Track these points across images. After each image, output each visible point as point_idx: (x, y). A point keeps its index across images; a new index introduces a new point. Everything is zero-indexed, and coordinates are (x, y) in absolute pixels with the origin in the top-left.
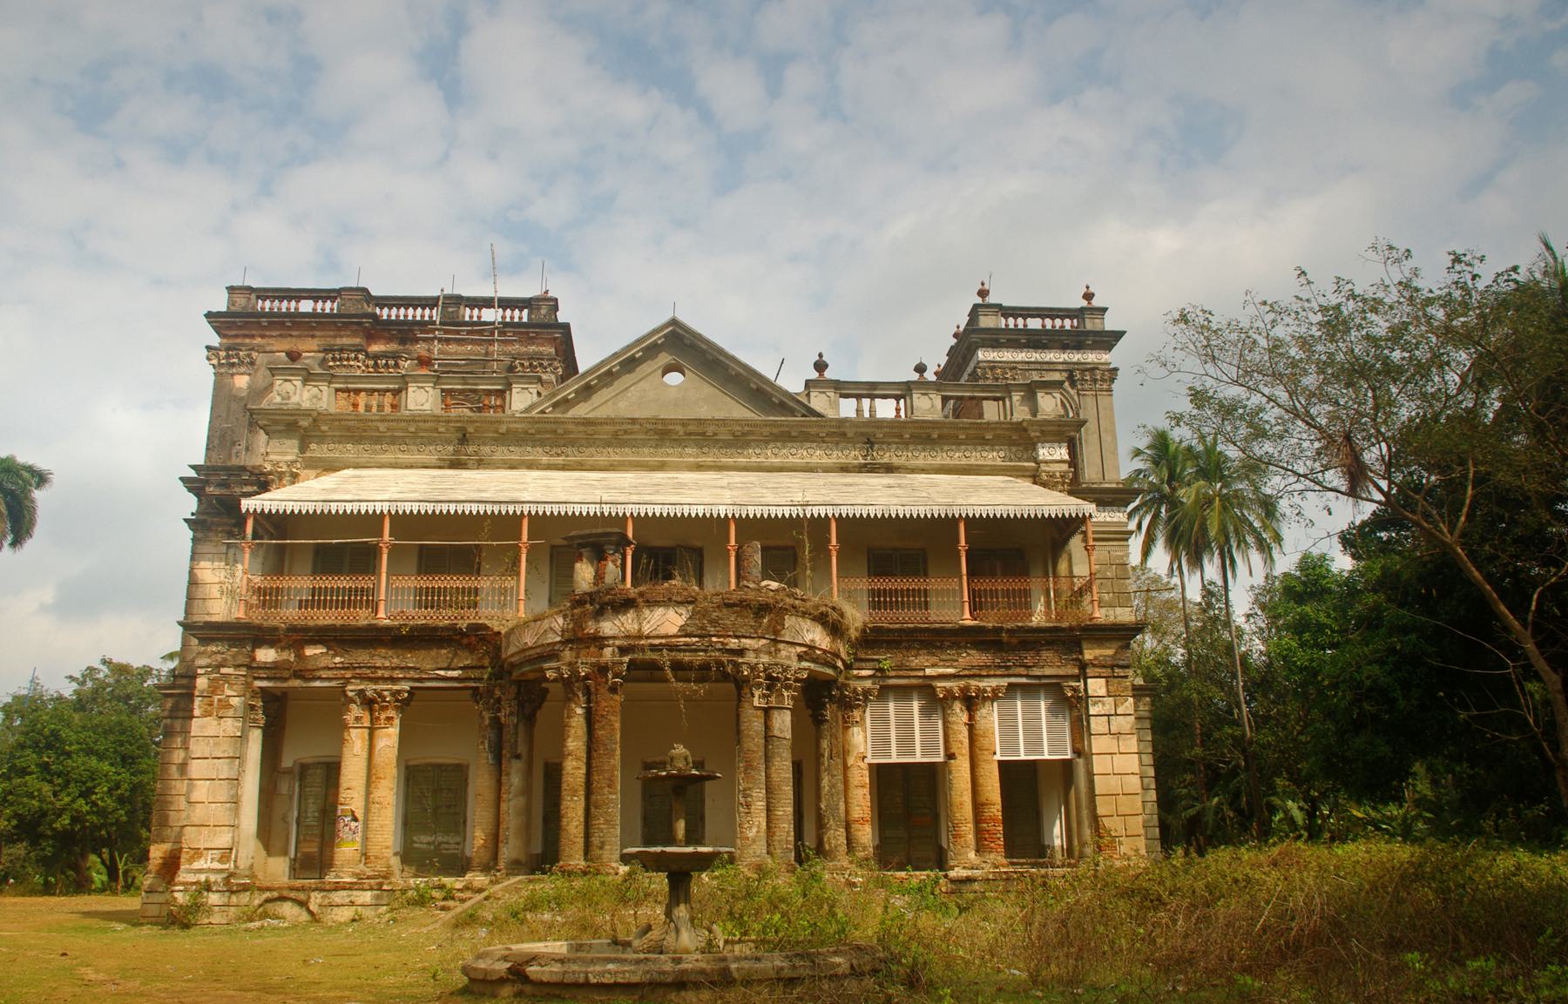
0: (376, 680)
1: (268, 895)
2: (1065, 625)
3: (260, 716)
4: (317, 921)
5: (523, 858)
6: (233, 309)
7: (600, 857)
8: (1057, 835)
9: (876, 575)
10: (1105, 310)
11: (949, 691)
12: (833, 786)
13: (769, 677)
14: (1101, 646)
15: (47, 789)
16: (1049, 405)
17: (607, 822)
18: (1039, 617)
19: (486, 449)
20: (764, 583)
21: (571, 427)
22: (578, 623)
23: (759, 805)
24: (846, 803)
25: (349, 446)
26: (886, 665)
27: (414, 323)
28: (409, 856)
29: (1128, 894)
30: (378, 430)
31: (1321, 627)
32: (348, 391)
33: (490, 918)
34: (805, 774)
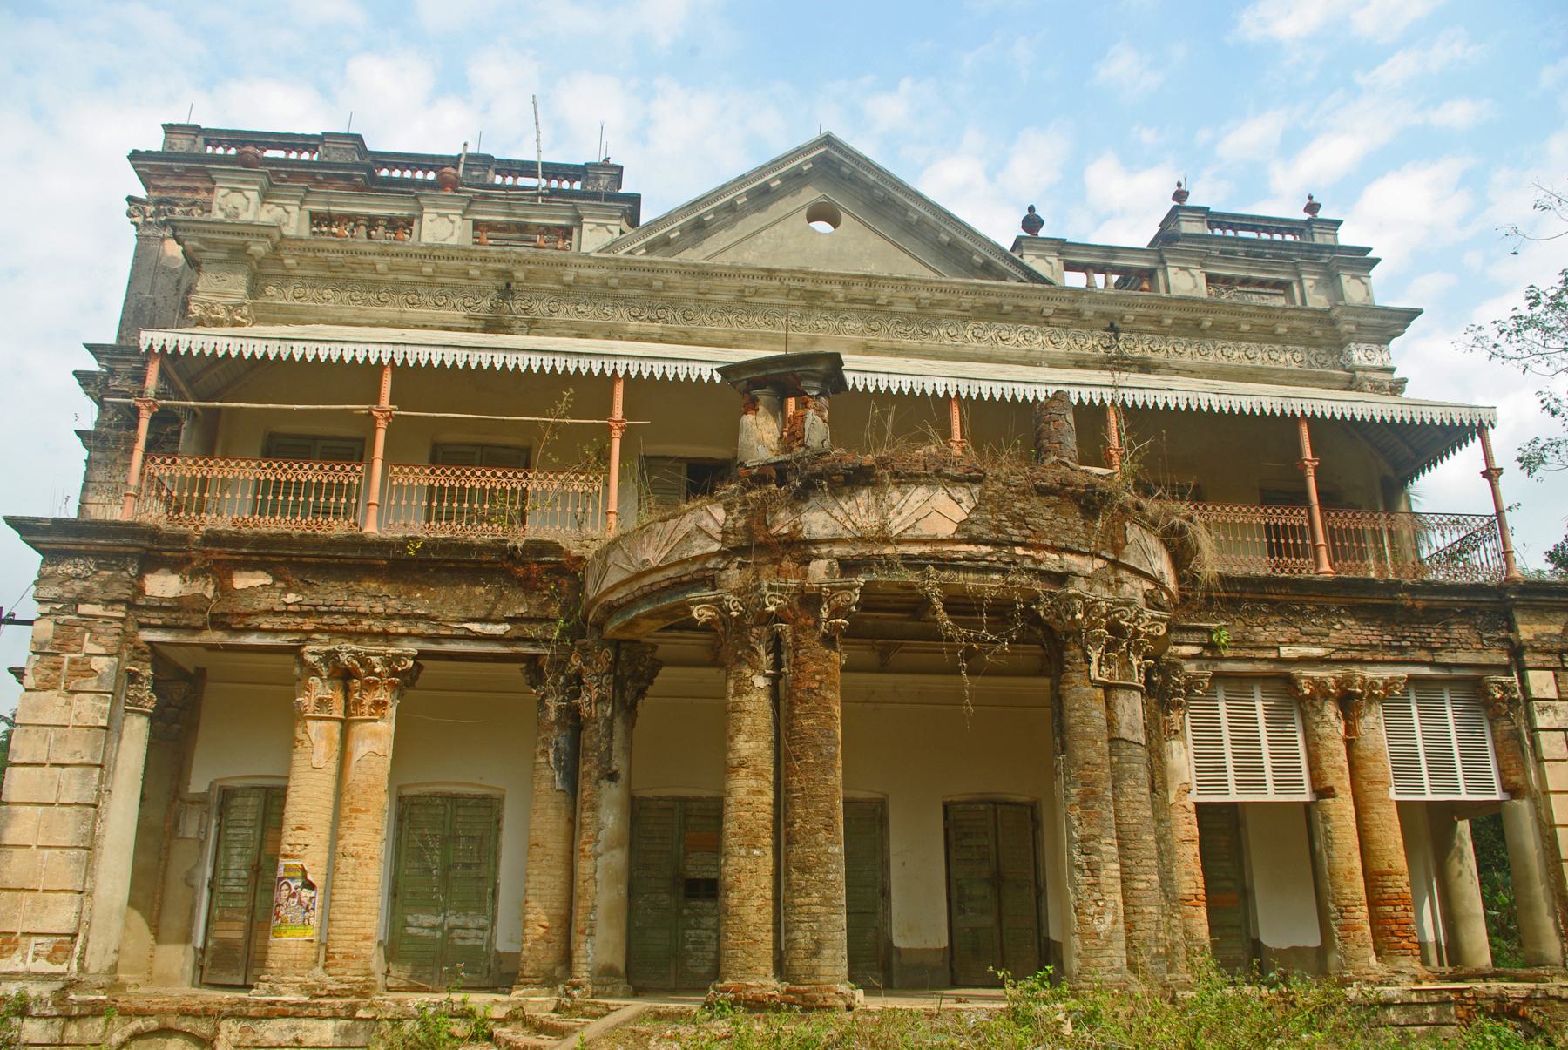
0: (357, 636)
1: (138, 1024)
7: (813, 973)
11: (1319, 685)
14: (1542, 620)
17: (826, 900)
19: (541, 308)
21: (674, 278)
25: (328, 293)
26: (1225, 637)
28: (394, 949)
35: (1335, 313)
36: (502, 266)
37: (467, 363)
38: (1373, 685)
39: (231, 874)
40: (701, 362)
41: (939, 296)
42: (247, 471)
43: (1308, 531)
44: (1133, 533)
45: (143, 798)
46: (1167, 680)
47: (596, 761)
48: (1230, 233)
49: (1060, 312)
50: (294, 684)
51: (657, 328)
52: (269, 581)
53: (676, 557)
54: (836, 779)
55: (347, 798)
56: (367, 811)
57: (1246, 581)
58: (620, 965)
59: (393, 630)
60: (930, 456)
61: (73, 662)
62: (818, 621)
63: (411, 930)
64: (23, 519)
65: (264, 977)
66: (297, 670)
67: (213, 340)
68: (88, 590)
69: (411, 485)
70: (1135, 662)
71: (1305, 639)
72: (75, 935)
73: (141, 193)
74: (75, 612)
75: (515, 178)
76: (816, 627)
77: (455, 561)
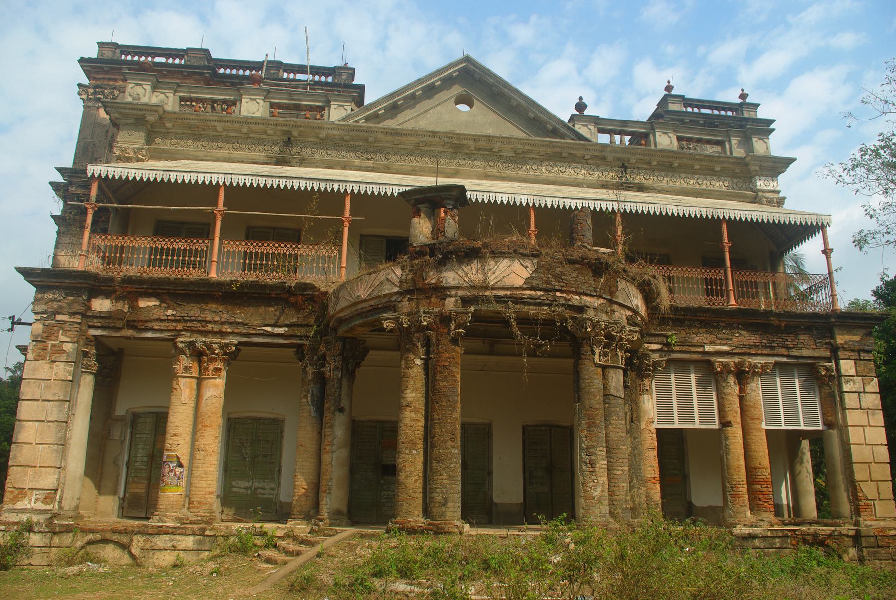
4: (139, 565)
7: (442, 515)
11: (725, 366)
14: (849, 333)
17: (450, 477)
19: (307, 152)
21: (381, 136)
22: (419, 273)
23: (602, 464)
25: (190, 142)
26: (675, 339)
28: (226, 498)
33: (330, 582)
35: (748, 159)
36: (286, 129)
37: (265, 184)
38: (755, 367)
39: (138, 459)
40: (392, 183)
41: (527, 147)
42: (144, 243)
43: (724, 282)
44: (622, 284)
45: (91, 418)
46: (641, 363)
47: (332, 402)
48: (696, 110)
49: (594, 157)
52: (158, 303)
53: (375, 294)
54: (457, 414)
55: (200, 419)
56: (211, 426)
57: (688, 310)
58: (345, 509)
59: (224, 330)
60: (512, 242)
61: (53, 345)
62: (450, 330)
63: (234, 490)
64: (25, 269)
65: (156, 513)
66: (173, 351)
67: (127, 170)
68: (61, 307)
69: (234, 252)
70: (620, 354)
71: (718, 341)
72: (56, 490)
73: (86, 81)
74: (54, 319)
75: (295, 74)
76: (448, 333)
77: (259, 294)
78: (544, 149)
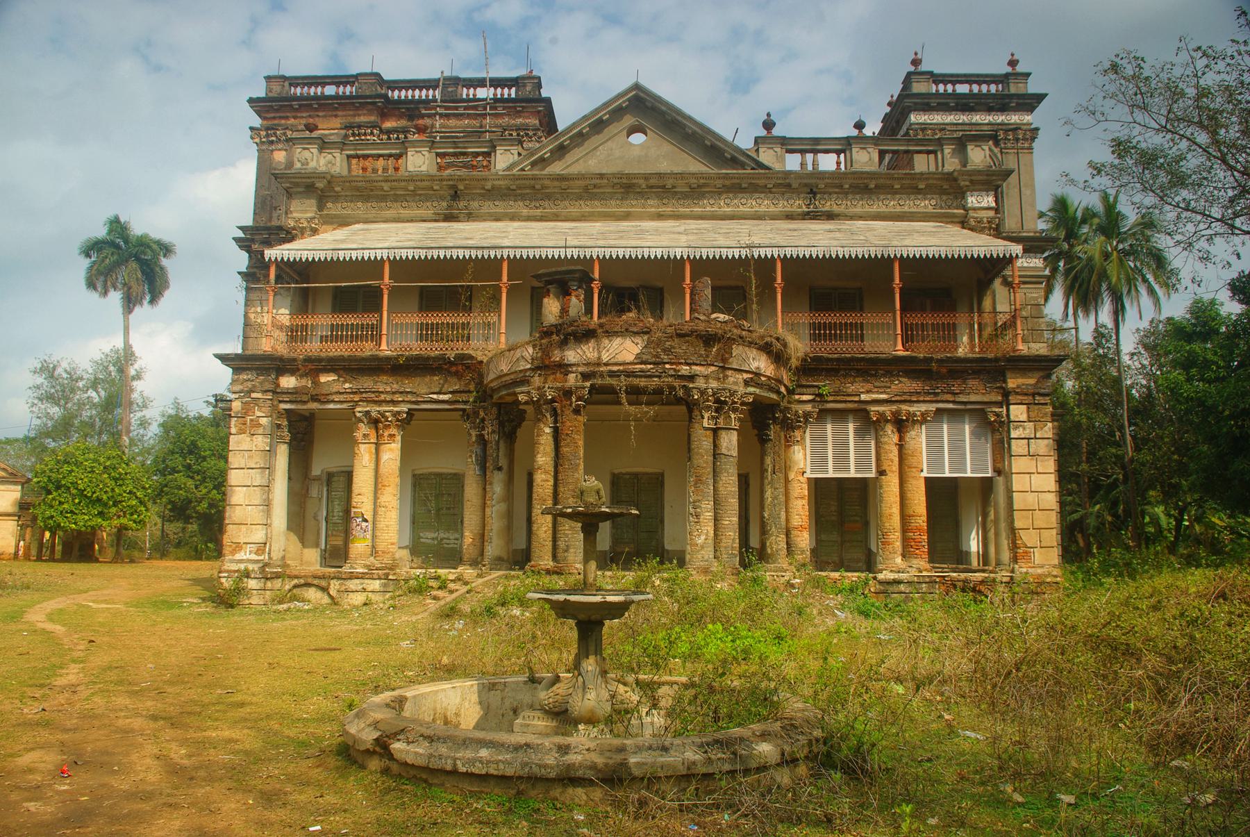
0: (380, 403)
1: (296, 581)
2: (991, 356)
3: (286, 434)
5: (504, 555)
6: (270, 95)
7: (565, 559)
8: (974, 544)
9: (817, 310)
10: (1028, 75)
11: (882, 415)
12: (775, 498)
13: (717, 401)
15: (190, 483)
16: (978, 156)
18: (964, 348)
19: (475, 204)
20: (714, 316)
21: (547, 182)
22: (546, 352)
24: (787, 512)
26: (825, 391)
27: (420, 101)
28: (416, 549)
29: (1094, 643)
30: (382, 189)
31: (1206, 364)
32: (358, 157)
34: (749, 488)
50: (352, 429)
51: (538, 212)
68: (254, 386)
78: (721, 182)
